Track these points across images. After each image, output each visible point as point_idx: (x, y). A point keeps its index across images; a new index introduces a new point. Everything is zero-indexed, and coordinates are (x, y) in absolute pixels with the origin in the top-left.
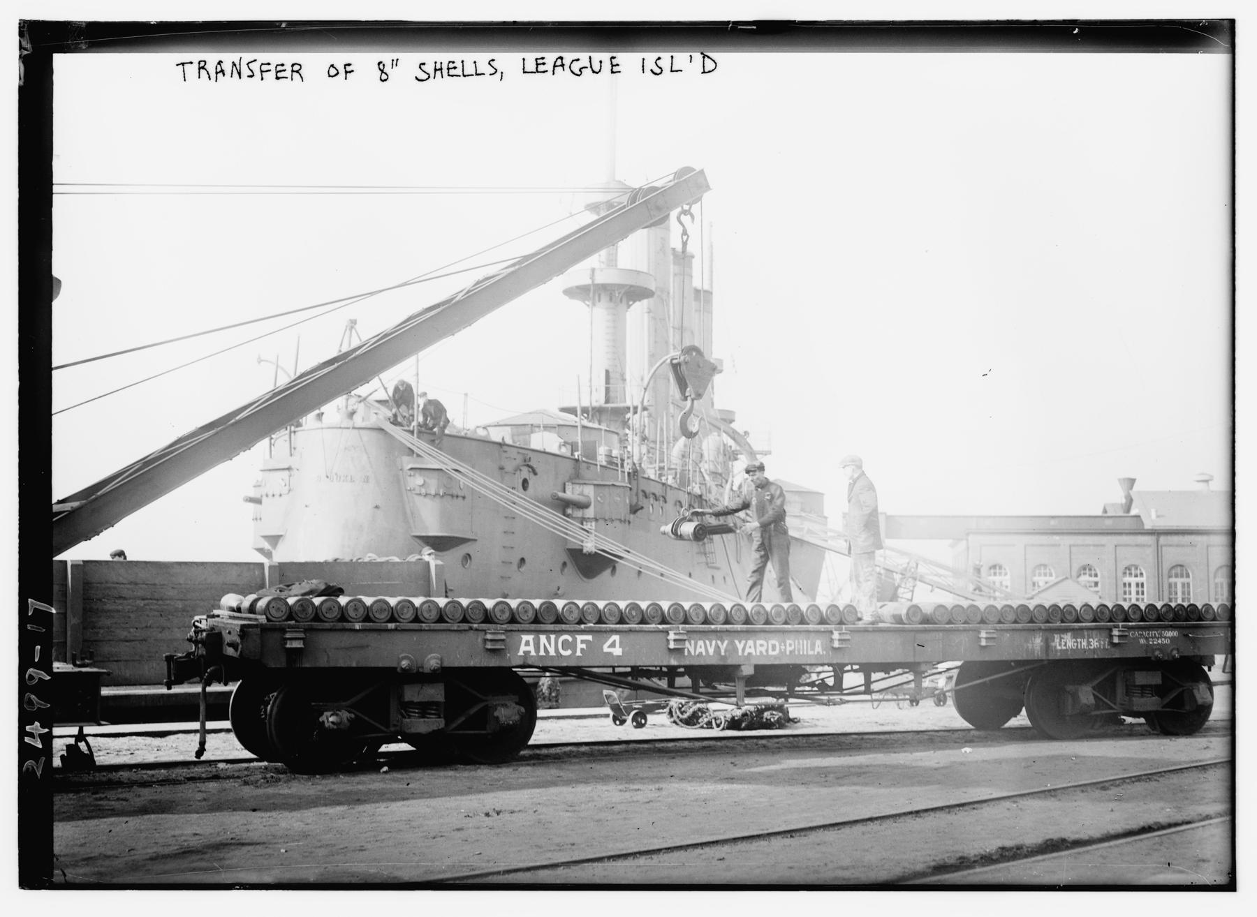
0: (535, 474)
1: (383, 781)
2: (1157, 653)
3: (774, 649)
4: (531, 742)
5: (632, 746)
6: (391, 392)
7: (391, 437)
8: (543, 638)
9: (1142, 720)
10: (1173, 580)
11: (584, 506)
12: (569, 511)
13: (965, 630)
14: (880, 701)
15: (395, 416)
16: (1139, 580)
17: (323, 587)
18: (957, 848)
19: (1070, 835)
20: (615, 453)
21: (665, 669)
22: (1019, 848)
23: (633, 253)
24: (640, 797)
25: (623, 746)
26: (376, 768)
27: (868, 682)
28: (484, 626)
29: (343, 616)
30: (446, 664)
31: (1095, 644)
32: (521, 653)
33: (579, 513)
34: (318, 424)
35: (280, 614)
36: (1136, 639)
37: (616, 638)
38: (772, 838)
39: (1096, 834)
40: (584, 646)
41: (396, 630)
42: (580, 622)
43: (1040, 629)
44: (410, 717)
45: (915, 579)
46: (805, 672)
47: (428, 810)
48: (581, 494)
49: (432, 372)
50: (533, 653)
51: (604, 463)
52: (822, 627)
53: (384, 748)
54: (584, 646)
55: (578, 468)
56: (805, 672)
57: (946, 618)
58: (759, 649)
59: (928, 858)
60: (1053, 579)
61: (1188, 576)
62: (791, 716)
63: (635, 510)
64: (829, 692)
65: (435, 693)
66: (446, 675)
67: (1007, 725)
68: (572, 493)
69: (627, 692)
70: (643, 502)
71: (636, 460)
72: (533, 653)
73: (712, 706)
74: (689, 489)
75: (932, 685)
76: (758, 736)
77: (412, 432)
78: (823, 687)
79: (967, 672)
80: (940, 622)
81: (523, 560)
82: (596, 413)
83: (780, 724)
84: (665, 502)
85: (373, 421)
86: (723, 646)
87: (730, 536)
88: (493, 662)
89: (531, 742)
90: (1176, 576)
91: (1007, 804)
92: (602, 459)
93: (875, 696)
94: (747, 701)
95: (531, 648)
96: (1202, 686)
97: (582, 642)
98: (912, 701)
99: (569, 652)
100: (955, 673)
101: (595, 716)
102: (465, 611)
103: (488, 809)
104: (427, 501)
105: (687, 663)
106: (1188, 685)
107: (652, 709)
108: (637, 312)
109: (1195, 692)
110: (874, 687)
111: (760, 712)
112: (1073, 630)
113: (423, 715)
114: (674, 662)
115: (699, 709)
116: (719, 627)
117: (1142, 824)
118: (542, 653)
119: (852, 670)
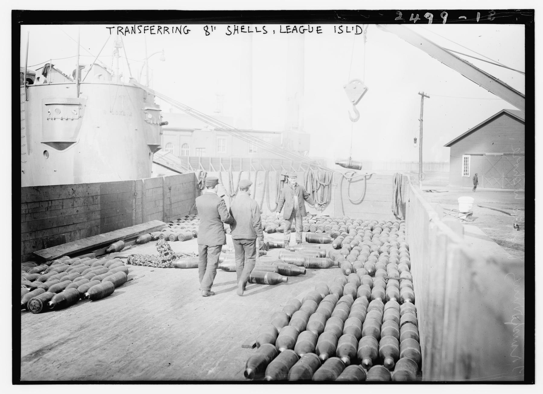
10: (183, 149)
48: (315, 324)
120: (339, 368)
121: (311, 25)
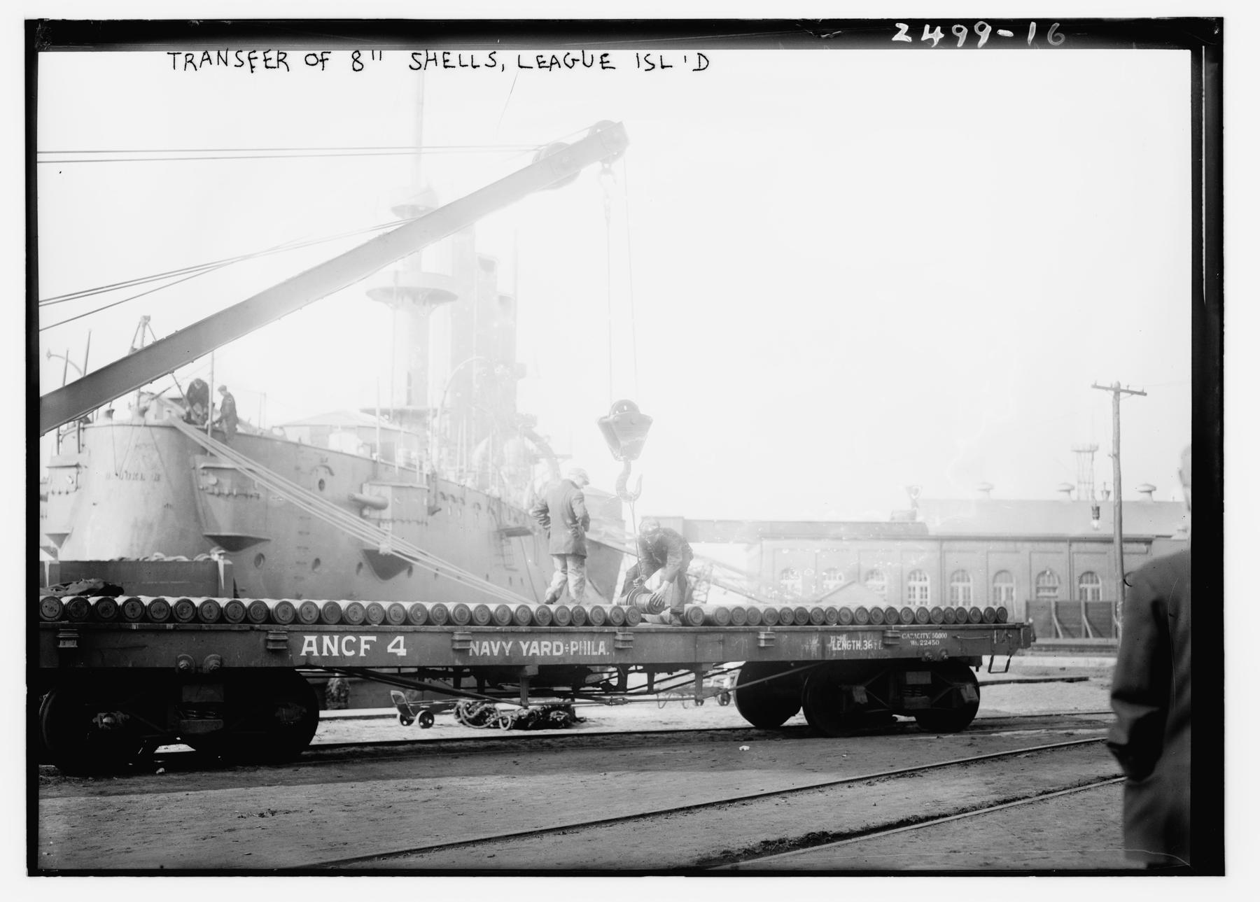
0: (332, 474)
1: (158, 782)
2: (927, 654)
3: (558, 650)
4: (314, 741)
5: (417, 746)
6: (185, 391)
7: (184, 436)
8: (326, 639)
9: (913, 719)
10: (955, 584)
11: (380, 507)
12: (366, 512)
13: (745, 632)
14: (666, 700)
15: (189, 414)
16: (923, 584)
17: (101, 586)
18: (725, 842)
19: (832, 829)
20: (414, 454)
21: (451, 670)
22: (781, 841)
23: (434, 259)
24: (419, 796)
25: (408, 746)
26: (151, 771)
27: (651, 682)
28: (266, 627)
29: (222, 616)
30: (226, 664)
31: (868, 645)
32: (303, 654)
33: (376, 514)
34: (109, 421)
35: (52, 614)
36: (908, 641)
37: (401, 638)
38: (545, 836)
39: (857, 827)
40: (368, 647)
41: (174, 630)
42: (365, 623)
43: (817, 631)
44: (187, 718)
45: (708, 582)
46: (591, 672)
47: (201, 811)
48: (379, 495)
49: (226, 369)
50: (316, 654)
51: (403, 465)
52: (606, 629)
53: (162, 749)
54: (368, 647)
55: (375, 471)
56: (591, 672)
57: (726, 620)
58: (543, 649)
59: (695, 853)
60: (842, 582)
61: (1097, 582)
62: (578, 714)
63: (433, 511)
64: (615, 692)
65: (211, 694)
66: (224, 674)
67: (787, 723)
68: (369, 494)
69: (416, 693)
70: (441, 503)
71: (435, 461)
72: (316, 654)
73: (499, 706)
74: (487, 491)
75: (717, 685)
76: (548, 738)
77: (206, 431)
78: (608, 688)
79: (748, 672)
80: (721, 624)
81: (317, 561)
82: (400, 415)
83: (567, 724)
84: (464, 503)
85: (165, 418)
86: (508, 647)
87: (529, 538)
88: (275, 663)
89: (314, 741)
90: (958, 580)
91: (776, 799)
92: (400, 461)
93: (661, 696)
94: (536, 701)
95: (314, 649)
96: (969, 686)
97: (366, 642)
98: (697, 701)
99: (352, 653)
100: (738, 671)
101: (383, 717)
102: (247, 611)
103: (263, 809)
104: (221, 501)
105: (471, 663)
106: (956, 684)
107: (439, 710)
108: (440, 315)
109: (963, 691)
110: (656, 687)
111: (546, 712)
112: (848, 632)
113: (201, 716)
114: (458, 663)
115: (487, 709)
116: (504, 629)
117: (901, 818)
118: (325, 653)
119: (637, 671)
120: (504, 615)
121: (588, 53)
